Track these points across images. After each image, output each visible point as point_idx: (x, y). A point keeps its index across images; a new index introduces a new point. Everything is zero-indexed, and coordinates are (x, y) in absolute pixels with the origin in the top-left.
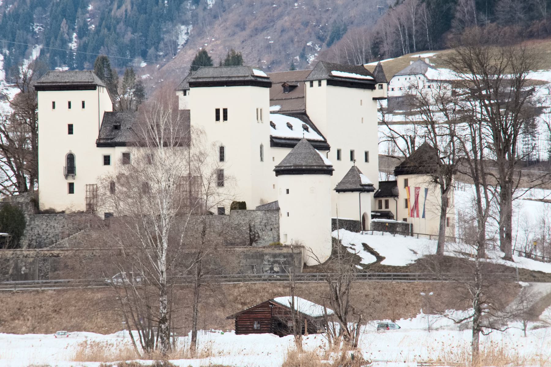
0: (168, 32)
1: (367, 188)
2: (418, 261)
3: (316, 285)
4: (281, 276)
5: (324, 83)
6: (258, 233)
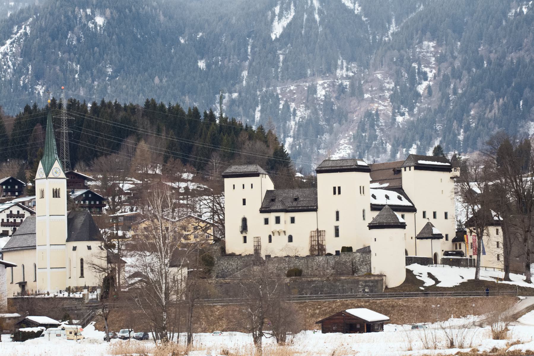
0: (522, 126)
1: (436, 236)
2: (463, 284)
3: (386, 300)
4: (370, 295)
5: (412, 168)
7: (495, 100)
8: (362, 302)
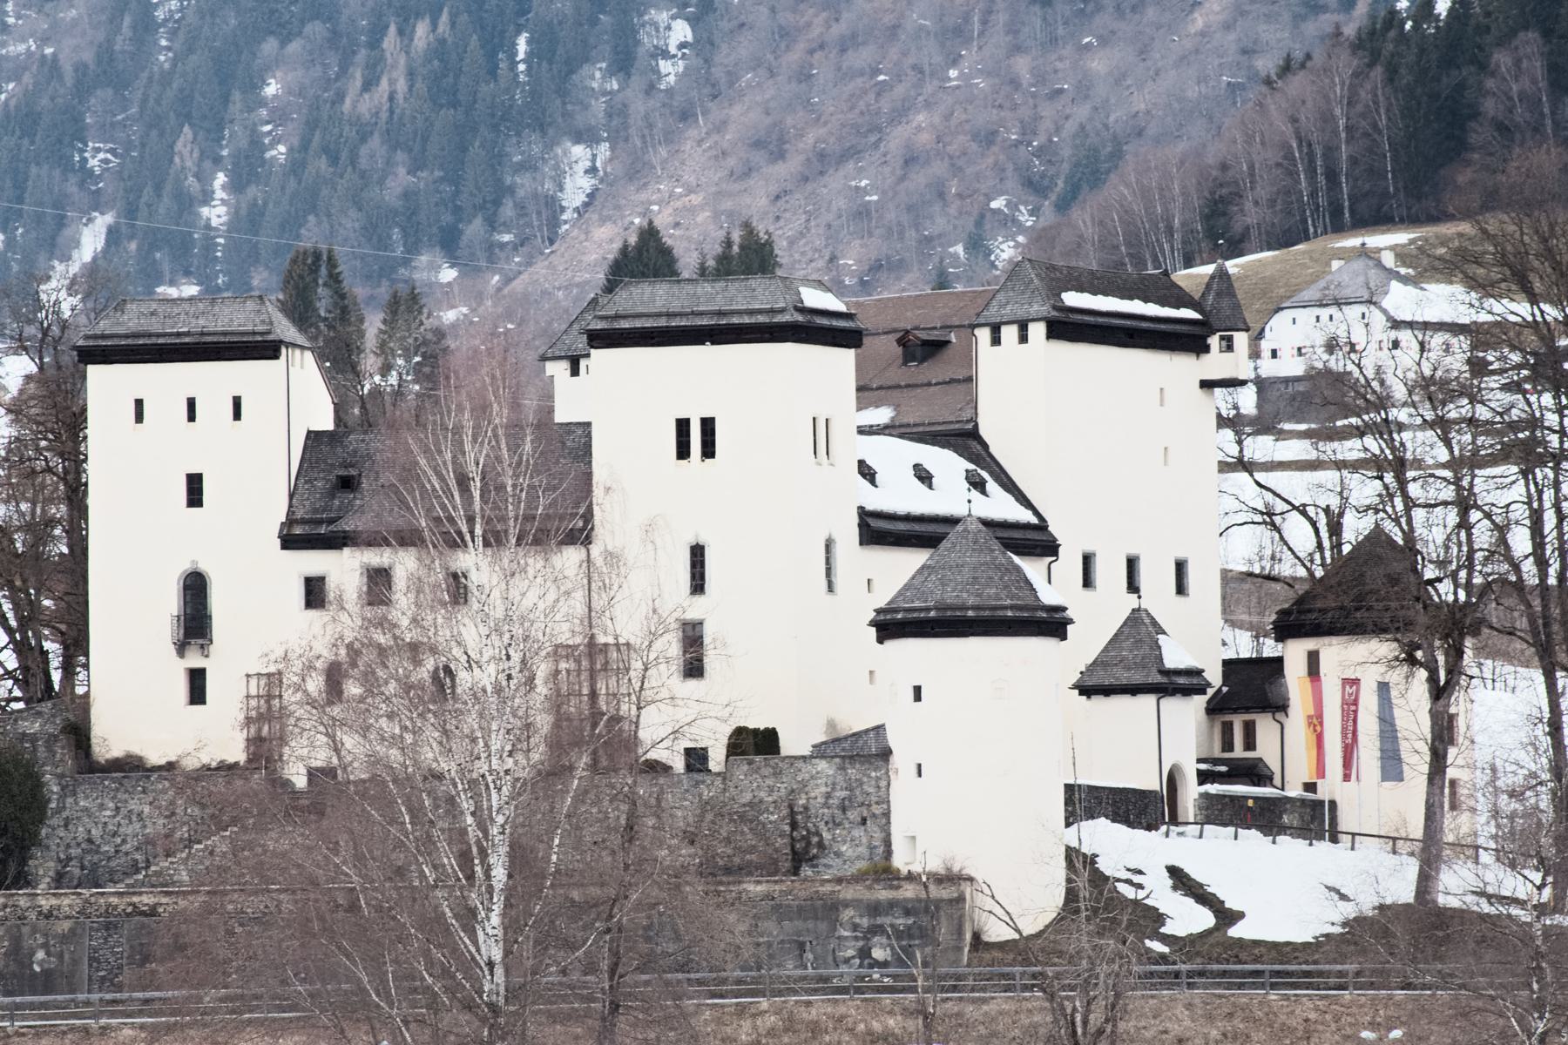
0: (528, 166)
1: (1181, 680)
4: (895, 977)
5: (1037, 330)
6: (818, 834)
7: (392, 29)
8: (891, 1013)
